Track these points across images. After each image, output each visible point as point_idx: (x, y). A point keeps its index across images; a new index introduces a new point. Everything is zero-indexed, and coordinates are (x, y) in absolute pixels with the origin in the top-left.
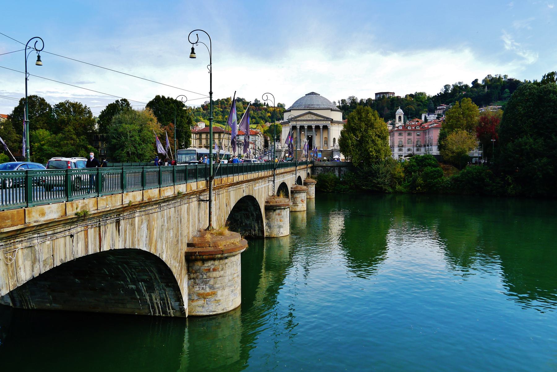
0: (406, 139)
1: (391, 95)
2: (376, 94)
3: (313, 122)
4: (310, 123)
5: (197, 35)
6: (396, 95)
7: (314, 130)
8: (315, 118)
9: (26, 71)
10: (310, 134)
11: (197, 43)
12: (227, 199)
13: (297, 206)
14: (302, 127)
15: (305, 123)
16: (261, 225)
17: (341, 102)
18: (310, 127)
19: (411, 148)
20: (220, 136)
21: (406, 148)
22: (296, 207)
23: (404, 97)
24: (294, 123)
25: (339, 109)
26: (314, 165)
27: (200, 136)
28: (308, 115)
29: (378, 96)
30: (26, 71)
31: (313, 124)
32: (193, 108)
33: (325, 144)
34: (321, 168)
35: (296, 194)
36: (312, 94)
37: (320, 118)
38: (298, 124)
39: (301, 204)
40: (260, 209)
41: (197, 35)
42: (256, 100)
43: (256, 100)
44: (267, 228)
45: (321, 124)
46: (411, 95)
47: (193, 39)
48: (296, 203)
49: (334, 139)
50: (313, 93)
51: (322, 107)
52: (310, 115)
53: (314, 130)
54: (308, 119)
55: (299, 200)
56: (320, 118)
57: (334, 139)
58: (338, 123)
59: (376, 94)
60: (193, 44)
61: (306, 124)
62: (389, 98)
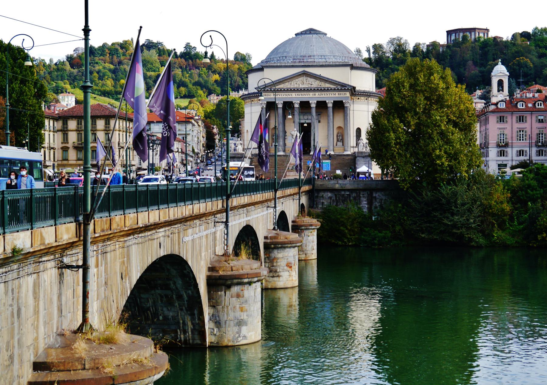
0: (515, 130)
1: (481, 35)
2: (449, 33)
3: (311, 94)
6: (491, 34)
7: (314, 111)
8: (315, 84)
10: (305, 120)
13: (278, 276)
14: (288, 106)
15: (294, 95)
16: (199, 319)
17: (372, 50)
18: (305, 106)
19: (524, 149)
20: (107, 123)
21: (515, 150)
22: (275, 279)
24: (271, 97)
25: (368, 66)
26: (313, 186)
27: (65, 124)
28: (301, 79)
29: (453, 37)
31: (313, 98)
32: (48, 62)
34: (330, 195)
35: (276, 251)
36: (310, 33)
37: (327, 85)
38: (280, 99)
40: (196, 285)
42: (188, 46)
43: (188, 46)
44: (212, 325)
45: (330, 98)
46: (525, 35)
48: (276, 271)
49: (359, 131)
50: (311, 31)
51: (331, 60)
52: (304, 78)
53: (314, 111)
54: (301, 86)
56: (327, 85)
57: (359, 131)
58: (367, 95)
59: (449, 33)
61: (296, 98)
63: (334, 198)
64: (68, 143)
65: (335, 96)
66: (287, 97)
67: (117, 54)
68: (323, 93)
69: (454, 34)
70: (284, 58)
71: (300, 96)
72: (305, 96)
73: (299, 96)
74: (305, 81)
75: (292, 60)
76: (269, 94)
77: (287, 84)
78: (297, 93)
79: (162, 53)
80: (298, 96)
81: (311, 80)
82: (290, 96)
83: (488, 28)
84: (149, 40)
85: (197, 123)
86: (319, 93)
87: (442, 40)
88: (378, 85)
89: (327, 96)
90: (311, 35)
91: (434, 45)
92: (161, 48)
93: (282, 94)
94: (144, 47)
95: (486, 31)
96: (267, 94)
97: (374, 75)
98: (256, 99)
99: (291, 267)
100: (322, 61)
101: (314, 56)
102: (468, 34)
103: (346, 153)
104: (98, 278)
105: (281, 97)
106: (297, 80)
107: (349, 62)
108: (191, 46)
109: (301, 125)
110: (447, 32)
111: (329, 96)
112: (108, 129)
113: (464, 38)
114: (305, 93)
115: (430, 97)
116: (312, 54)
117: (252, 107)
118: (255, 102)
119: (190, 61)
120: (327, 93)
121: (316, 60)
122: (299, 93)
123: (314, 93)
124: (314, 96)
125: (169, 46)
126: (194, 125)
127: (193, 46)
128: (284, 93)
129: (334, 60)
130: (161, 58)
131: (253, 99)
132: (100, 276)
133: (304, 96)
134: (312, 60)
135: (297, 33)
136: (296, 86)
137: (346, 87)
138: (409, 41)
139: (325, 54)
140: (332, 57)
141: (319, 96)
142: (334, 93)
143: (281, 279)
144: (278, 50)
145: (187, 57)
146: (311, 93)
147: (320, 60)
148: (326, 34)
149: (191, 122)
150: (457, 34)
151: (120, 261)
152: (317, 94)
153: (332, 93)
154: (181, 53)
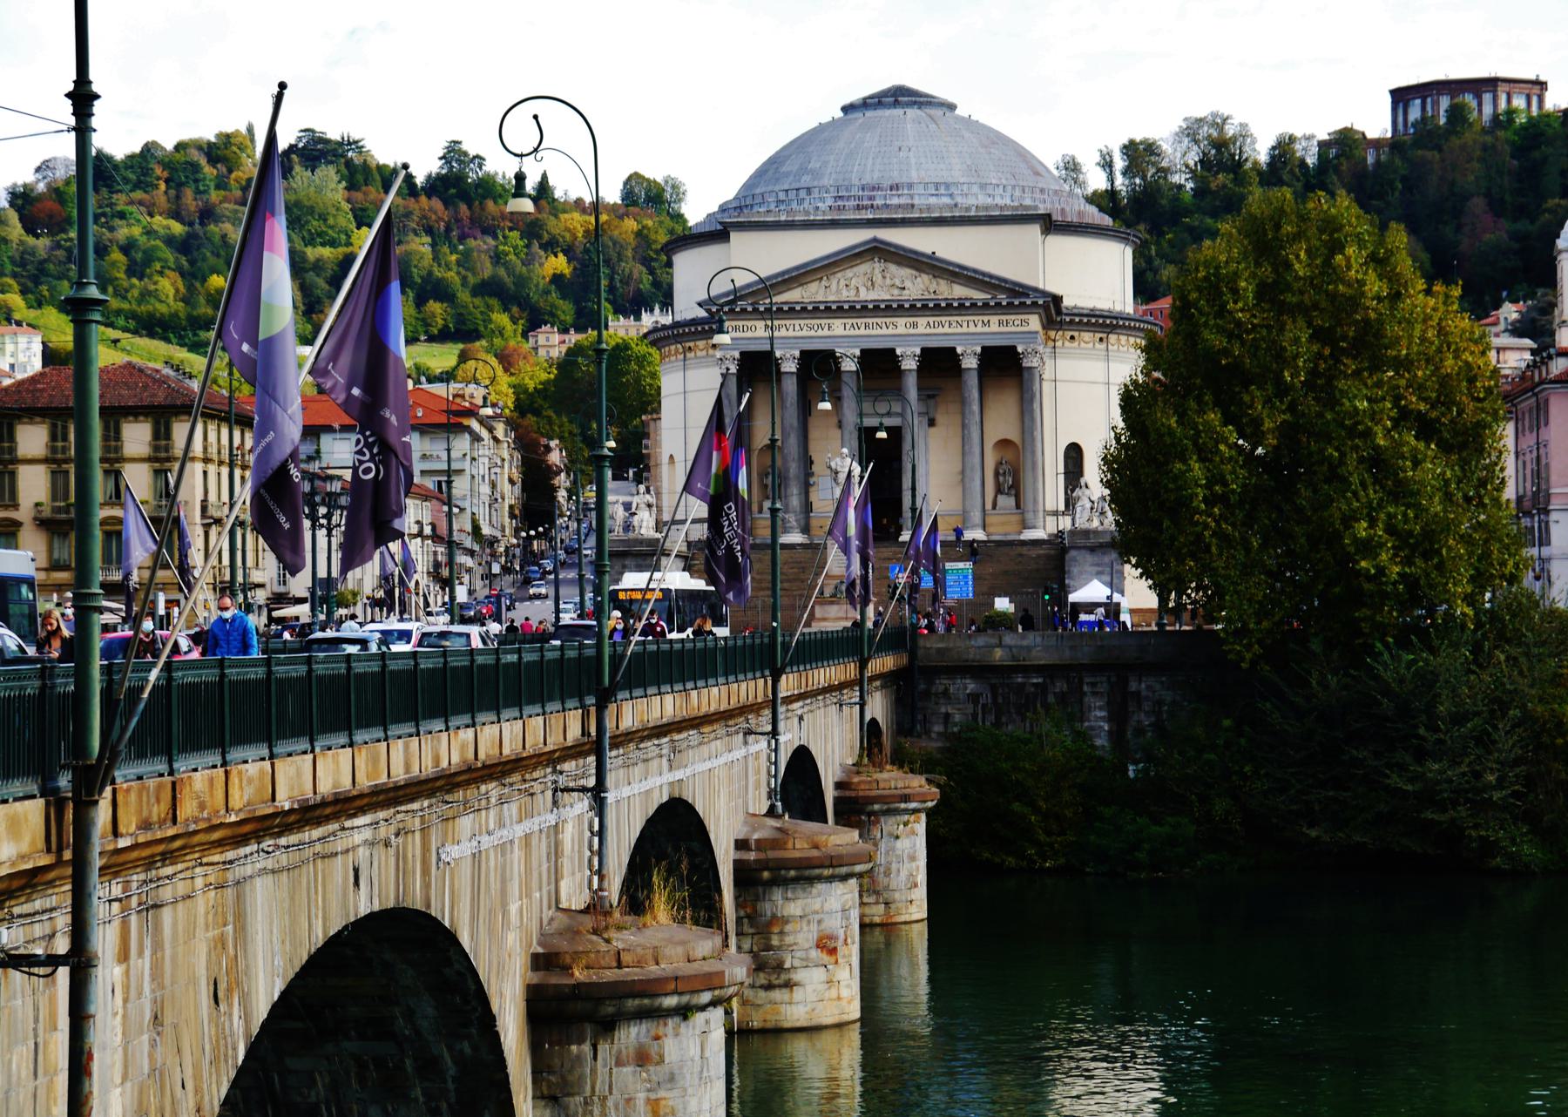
1: (1519, 102)
2: (1401, 96)
3: (901, 325)
4: (879, 332)
5: (536, 117)
7: (972, 382)
8: (917, 286)
10: (880, 418)
11: (536, 150)
12: (221, 941)
13: (789, 985)
15: (838, 327)
17: (1119, 163)
22: (777, 995)
23: (1389, 135)
24: (755, 333)
25: (1107, 221)
28: (865, 268)
29: (1415, 113)
36: (896, 104)
39: (818, 975)
41: (536, 117)
43: (454, 153)
49: (1074, 454)
50: (898, 97)
51: (971, 201)
52: (875, 267)
54: (865, 295)
55: (801, 938)
57: (1074, 454)
58: (1103, 324)
59: (1401, 96)
60: (521, 156)
62: (1503, 121)
63: (986, 698)
64: (16, 506)
65: (986, 329)
66: (812, 333)
69: (1418, 102)
70: (803, 194)
72: (879, 332)
73: (857, 332)
74: (878, 278)
76: (749, 323)
77: (813, 287)
78: (850, 321)
79: (360, 178)
80: (852, 332)
81: (901, 274)
82: (826, 332)
83: (1542, 78)
84: (313, 131)
85: (491, 430)
86: (931, 320)
87: (1376, 123)
88: (1144, 288)
89: (959, 330)
91: (1346, 141)
95: (1536, 89)
96: (740, 323)
97: (1129, 252)
98: (701, 344)
99: (833, 951)
100: (939, 203)
101: (910, 186)
102: (1469, 99)
103: (1029, 535)
104: (126, 1001)
105: (791, 333)
106: (849, 273)
109: (866, 434)
111: (965, 329)
112: (163, 455)
113: (1456, 113)
114: (879, 320)
116: (904, 180)
117: (689, 373)
118: (699, 354)
124: (912, 331)
125: (384, 153)
126: (476, 438)
128: (802, 322)
129: (983, 200)
130: (358, 196)
131: (691, 344)
132: (133, 994)
134: (903, 201)
136: (847, 295)
137: (1027, 296)
138: (1254, 129)
139: (950, 180)
140: (975, 189)
141: (928, 331)
142: (986, 318)
143: (798, 994)
145: (453, 191)
146: (901, 321)
147: (933, 200)
148: (952, 107)
149: (468, 429)
150: (1429, 100)
151: (210, 934)
152: (923, 324)
153: (976, 318)
154: (429, 177)
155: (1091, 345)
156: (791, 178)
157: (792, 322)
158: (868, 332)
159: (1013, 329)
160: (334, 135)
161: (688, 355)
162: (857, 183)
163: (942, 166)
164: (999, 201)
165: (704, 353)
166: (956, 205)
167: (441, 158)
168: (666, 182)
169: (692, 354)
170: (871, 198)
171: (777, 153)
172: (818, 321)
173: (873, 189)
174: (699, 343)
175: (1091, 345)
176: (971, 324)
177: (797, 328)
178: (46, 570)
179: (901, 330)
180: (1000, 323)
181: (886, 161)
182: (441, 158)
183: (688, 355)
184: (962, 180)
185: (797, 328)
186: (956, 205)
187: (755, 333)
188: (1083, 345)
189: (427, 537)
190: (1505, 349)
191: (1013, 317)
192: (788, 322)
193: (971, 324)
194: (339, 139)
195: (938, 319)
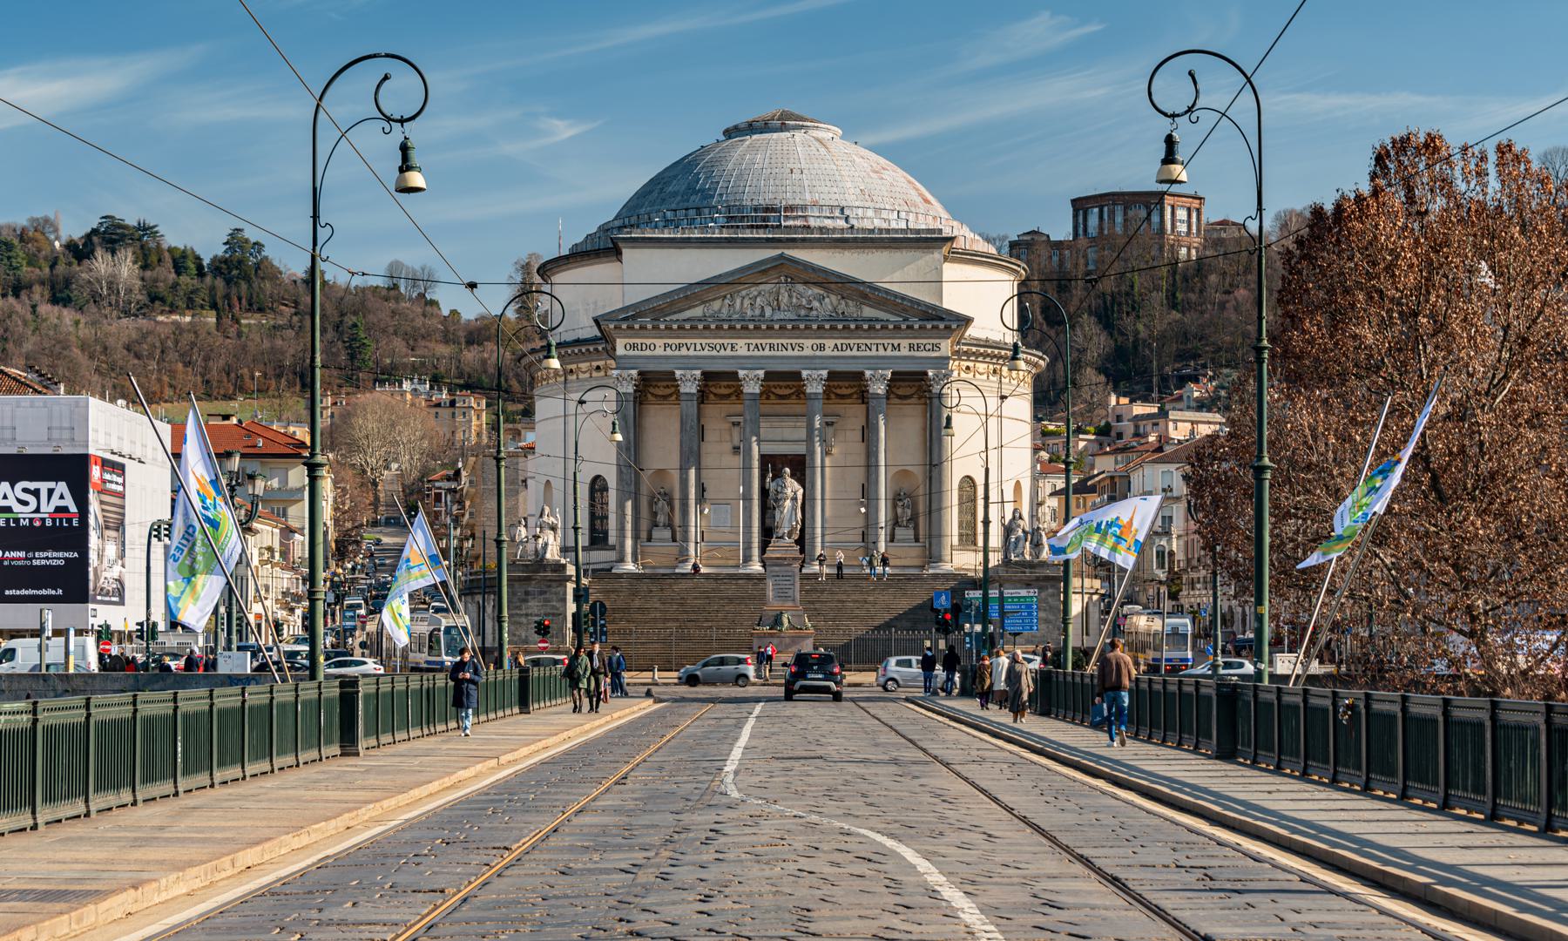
2: (1081, 206)
9: (315, 217)
11: (1190, 110)
24: (658, 349)
30: (315, 217)
33: (895, 522)
43: (235, 240)
47: (1173, 92)
51: (867, 225)
59: (1081, 206)
60: (1173, 116)
65: (896, 353)
66: (714, 353)
67: (9, 258)
68: (852, 342)
69: (1096, 210)
70: (692, 213)
71: (767, 352)
73: (761, 353)
75: (722, 221)
76: (648, 342)
78: (754, 341)
79: (154, 258)
80: (756, 353)
82: (729, 352)
83: (1200, 194)
84: (112, 217)
86: (839, 342)
89: (868, 353)
90: (788, 134)
92: (152, 245)
93: (698, 341)
94: (95, 239)
95: (1196, 204)
96: (639, 341)
98: (584, 366)
101: (804, 208)
107: (940, 231)
108: (247, 241)
110: (1074, 202)
111: (874, 353)
114: (784, 341)
115: (1503, 327)
116: (798, 202)
118: (581, 376)
119: (244, 286)
120: (868, 342)
121: (812, 223)
122: (764, 341)
123: (818, 341)
124: (818, 353)
125: (173, 237)
127: (253, 240)
128: (704, 341)
130: (148, 274)
131: (573, 367)
133: (779, 353)
134: (799, 223)
135: (730, 124)
137: (942, 319)
139: (844, 203)
140: (870, 213)
141: (836, 353)
142: (896, 342)
144: (667, 184)
145: (235, 272)
147: (828, 223)
150: (1106, 209)
153: (886, 342)
155: (985, 377)
156: (679, 198)
157: (694, 341)
158: (773, 353)
159: (924, 354)
160: (131, 221)
161: (569, 377)
162: (749, 203)
163: (835, 189)
164: (894, 225)
165: (587, 375)
166: (852, 227)
167: (225, 244)
168: (423, 270)
169: (574, 377)
170: (764, 219)
171: (659, 174)
172: (721, 341)
173: (767, 210)
174: (580, 365)
175: (985, 377)
176: (881, 347)
177: (698, 347)
178: (171, 816)
179: (808, 352)
180: (911, 347)
181: (777, 182)
182: (225, 244)
183: (569, 377)
184: (857, 204)
185: (698, 347)
186: (852, 227)
187: (658, 349)
188: (977, 376)
189: (277, 564)
190: (1198, 422)
191: (924, 341)
192: (689, 341)
193: (881, 347)
194: (136, 224)
195: (847, 341)
